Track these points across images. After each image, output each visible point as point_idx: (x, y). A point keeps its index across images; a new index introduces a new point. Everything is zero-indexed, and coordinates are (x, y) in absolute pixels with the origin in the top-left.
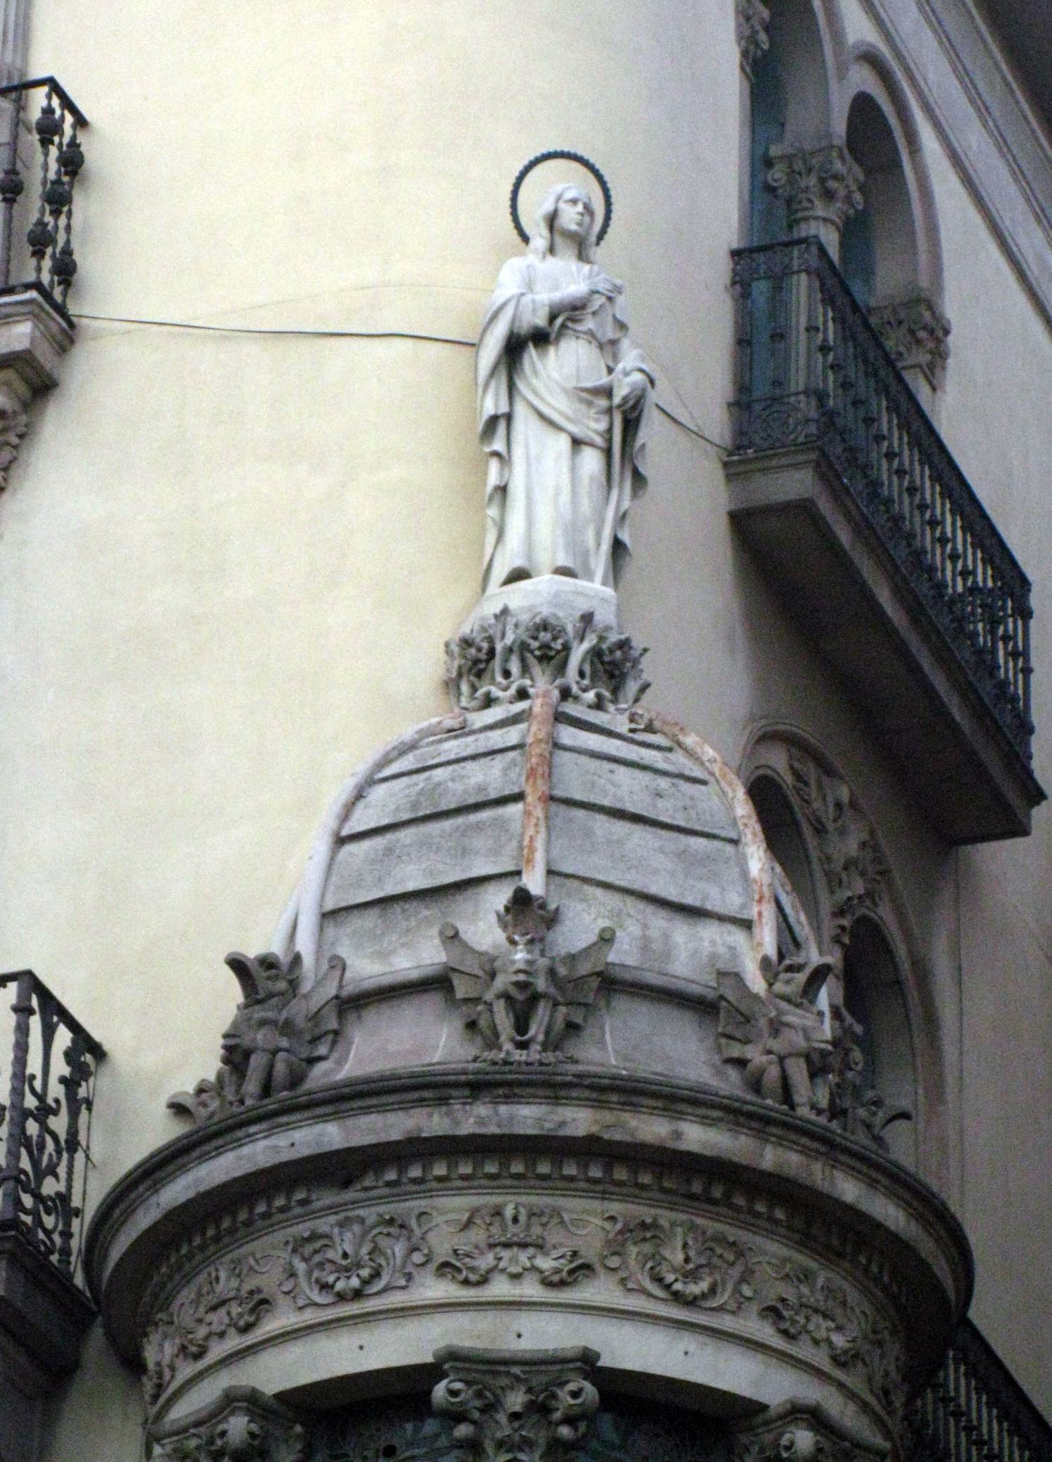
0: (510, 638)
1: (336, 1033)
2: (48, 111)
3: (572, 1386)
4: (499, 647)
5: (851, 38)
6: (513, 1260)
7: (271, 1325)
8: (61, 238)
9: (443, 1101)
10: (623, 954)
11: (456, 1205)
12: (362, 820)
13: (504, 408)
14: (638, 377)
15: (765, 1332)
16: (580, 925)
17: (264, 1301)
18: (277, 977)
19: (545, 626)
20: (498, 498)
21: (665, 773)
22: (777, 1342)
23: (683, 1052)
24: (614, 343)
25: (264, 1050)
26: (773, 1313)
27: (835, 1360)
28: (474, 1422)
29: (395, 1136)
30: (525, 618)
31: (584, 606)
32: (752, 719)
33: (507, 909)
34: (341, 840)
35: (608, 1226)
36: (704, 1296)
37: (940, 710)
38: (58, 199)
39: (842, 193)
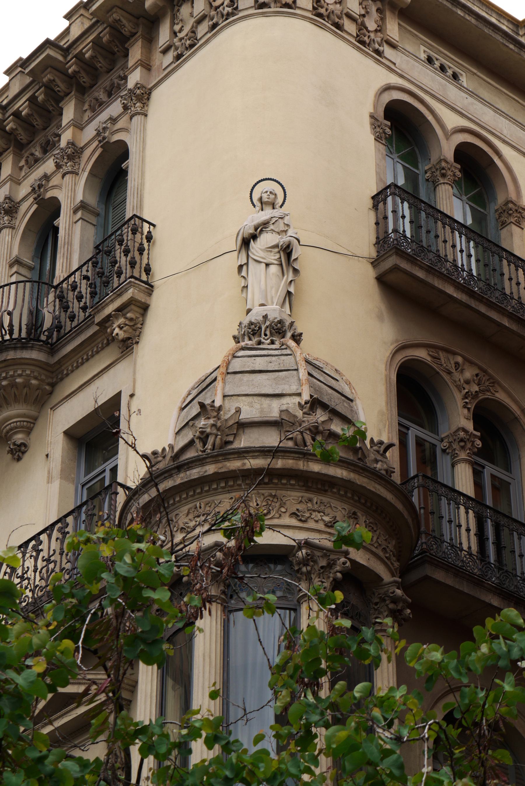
9: (171, 476)
15: (294, 522)
18: (158, 457)
27: (326, 525)
35: (230, 501)
37: (499, 325)
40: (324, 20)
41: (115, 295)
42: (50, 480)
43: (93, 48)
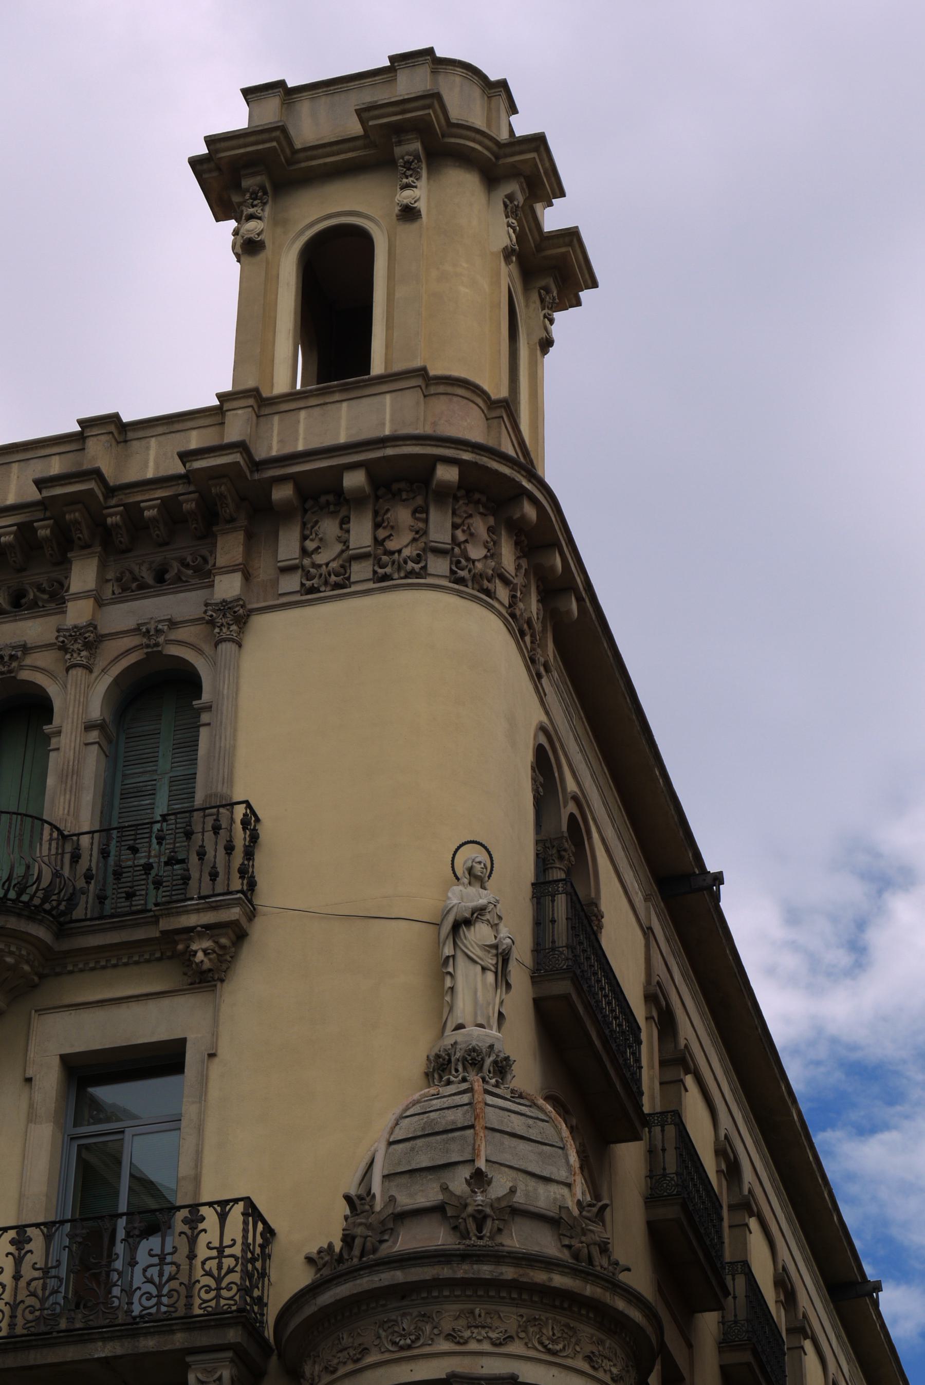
0: (458, 1055)
1: (392, 1229)
2: (245, 815)
4: (453, 1059)
5: (569, 790)
6: (479, 1333)
8: (250, 870)
9: (448, 1262)
11: (455, 1308)
12: (399, 1134)
13: (452, 953)
14: (509, 941)
15: (585, 1367)
17: (366, 1349)
19: (474, 1050)
21: (531, 1117)
23: (546, 1244)
24: (497, 925)
26: (589, 1358)
30: (463, 1046)
31: (489, 1041)
34: (390, 1144)
35: (519, 1319)
36: (561, 1351)
38: (249, 854)
39: (567, 857)
41: (206, 905)
42: (32, 1117)
43: (158, 507)
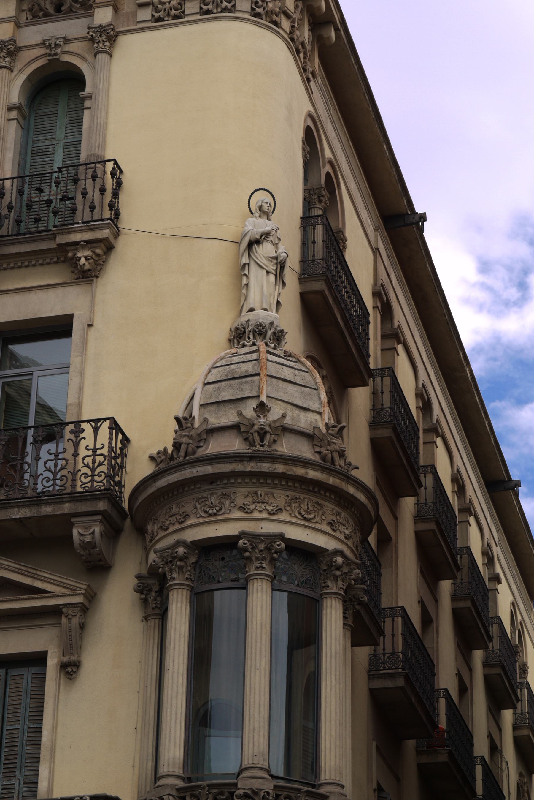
2: (113, 168)
3: (278, 543)
4: (247, 331)
5: (326, 156)
6: (260, 507)
7: (189, 522)
8: (116, 205)
9: (241, 461)
10: (288, 421)
12: (210, 379)
13: (247, 262)
14: (285, 254)
15: (328, 529)
16: (276, 412)
17: (187, 515)
18: (188, 423)
19: (260, 325)
20: (245, 287)
22: (332, 532)
23: (304, 450)
25: (185, 443)
26: (330, 524)
27: (346, 538)
28: (250, 552)
29: (228, 470)
30: (254, 322)
31: (271, 320)
32: (304, 352)
33: (257, 407)
35: (286, 498)
36: (312, 519)
38: (116, 194)
39: (324, 201)
40: (262, 19)
41: (87, 228)
